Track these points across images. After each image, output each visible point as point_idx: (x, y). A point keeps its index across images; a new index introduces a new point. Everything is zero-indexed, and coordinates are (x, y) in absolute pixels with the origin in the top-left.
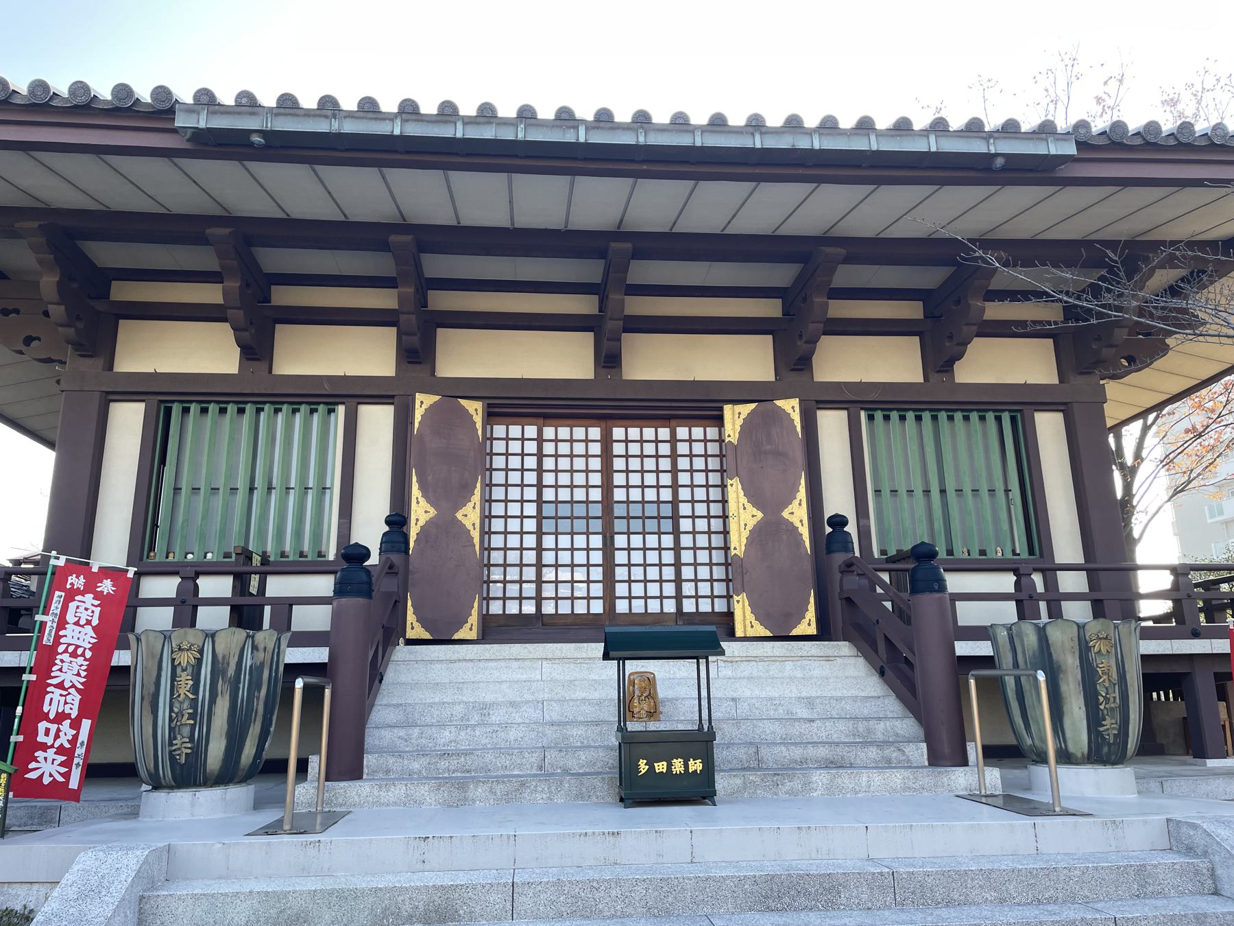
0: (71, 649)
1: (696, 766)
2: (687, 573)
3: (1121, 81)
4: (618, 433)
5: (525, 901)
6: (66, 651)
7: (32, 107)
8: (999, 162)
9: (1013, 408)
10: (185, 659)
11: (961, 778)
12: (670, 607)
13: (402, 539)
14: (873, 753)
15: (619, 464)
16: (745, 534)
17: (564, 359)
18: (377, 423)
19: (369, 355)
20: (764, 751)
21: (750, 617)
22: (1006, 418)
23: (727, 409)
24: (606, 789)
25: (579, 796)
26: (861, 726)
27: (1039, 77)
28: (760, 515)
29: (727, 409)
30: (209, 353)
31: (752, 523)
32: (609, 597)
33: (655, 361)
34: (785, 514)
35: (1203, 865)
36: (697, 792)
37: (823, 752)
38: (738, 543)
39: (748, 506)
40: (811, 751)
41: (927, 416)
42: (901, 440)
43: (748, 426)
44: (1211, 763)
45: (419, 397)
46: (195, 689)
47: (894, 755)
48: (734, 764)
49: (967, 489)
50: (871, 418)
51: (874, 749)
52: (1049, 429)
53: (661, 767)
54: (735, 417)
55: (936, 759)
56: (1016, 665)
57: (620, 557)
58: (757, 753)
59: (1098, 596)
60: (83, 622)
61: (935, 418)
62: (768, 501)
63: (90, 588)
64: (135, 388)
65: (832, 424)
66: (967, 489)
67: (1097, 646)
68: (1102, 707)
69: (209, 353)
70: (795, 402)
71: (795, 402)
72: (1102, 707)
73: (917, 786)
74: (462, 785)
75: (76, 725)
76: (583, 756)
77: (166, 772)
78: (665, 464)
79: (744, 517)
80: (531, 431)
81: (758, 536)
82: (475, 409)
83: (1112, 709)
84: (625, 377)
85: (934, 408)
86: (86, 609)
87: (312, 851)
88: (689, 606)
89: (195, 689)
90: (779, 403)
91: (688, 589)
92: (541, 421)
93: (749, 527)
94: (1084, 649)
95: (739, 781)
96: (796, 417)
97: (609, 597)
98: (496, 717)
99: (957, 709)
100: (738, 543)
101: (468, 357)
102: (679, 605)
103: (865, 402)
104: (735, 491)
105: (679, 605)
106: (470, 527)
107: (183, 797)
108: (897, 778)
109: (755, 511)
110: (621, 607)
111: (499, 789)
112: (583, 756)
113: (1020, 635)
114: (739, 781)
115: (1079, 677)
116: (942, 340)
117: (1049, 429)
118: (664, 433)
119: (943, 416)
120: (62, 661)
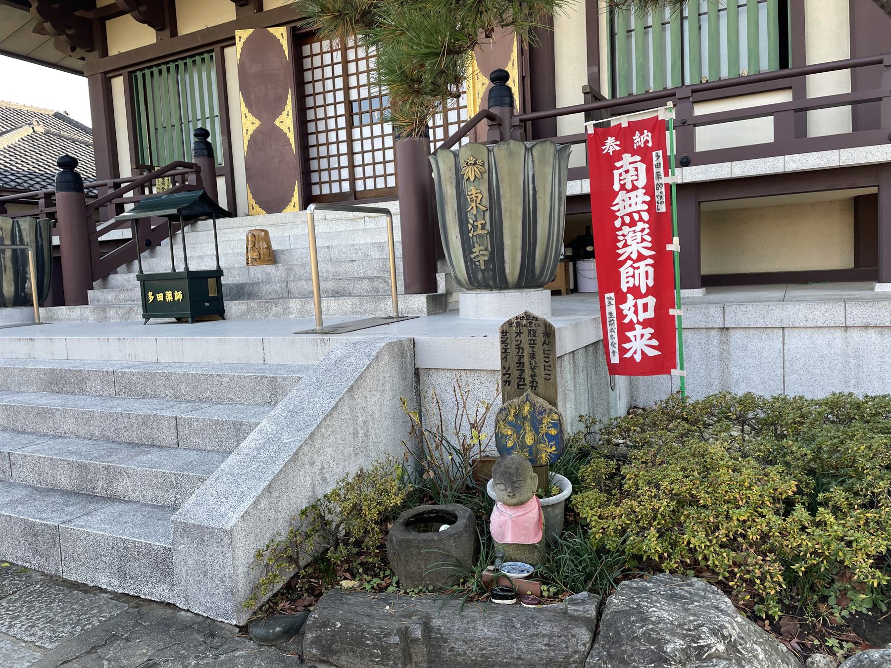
0: (627, 220)
6: (623, 223)
13: (507, 93)
16: (247, 138)
20: (292, 286)
31: (252, 129)
47: (381, 285)
48: (273, 295)
51: (366, 282)
53: (160, 297)
58: (287, 287)
60: (629, 186)
68: (471, 235)
72: (471, 235)
73: (362, 310)
83: (481, 236)
86: (627, 172)
90: (271, 30)
93: (250, 133)
95: (244, 307)
106: (286, 131)
109: (254, 119)
114: (244, 307)
115: (456, 206)
120: (624, 235)
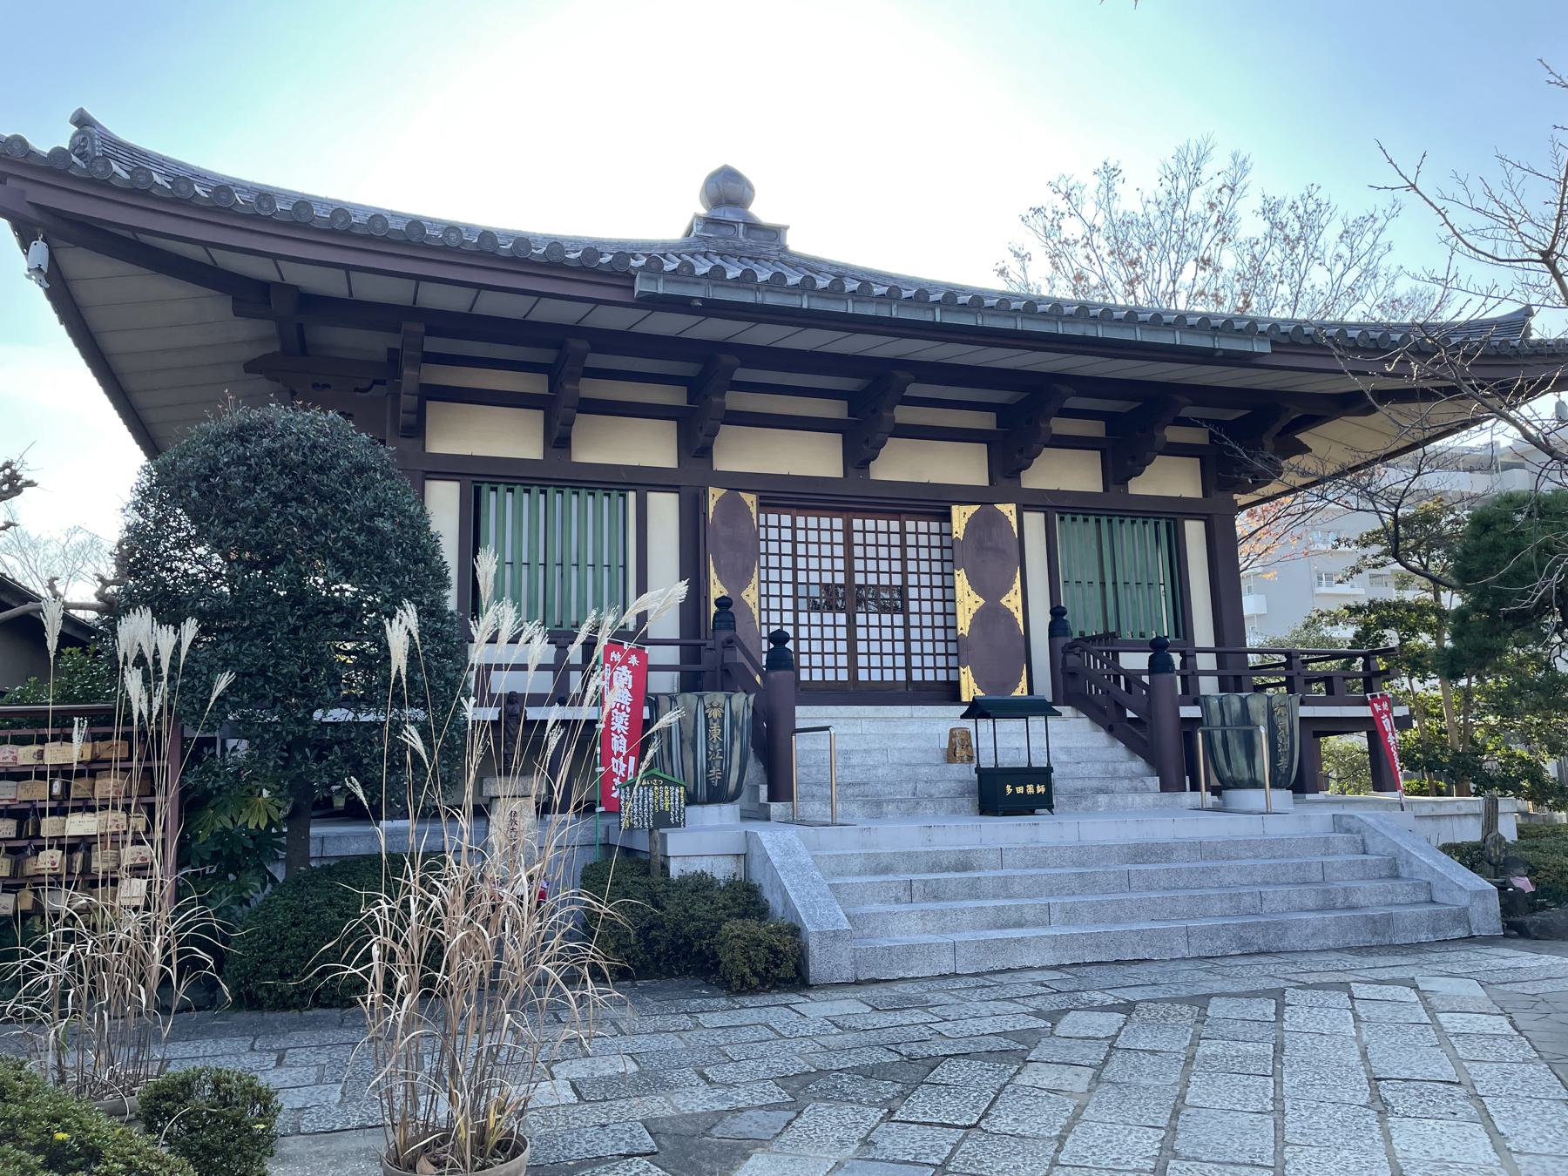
1: (1041, 789)
2: (915, 647)
3: (1232, 190)
4: (857, 524)
5: (1008, 859)
7: (513, 260)
8: (1220, 353)
9: (1169, 515)
10: (715, 713)
11: (1189, 798)
12: (901, 676)
14: (1126, 783)
15: (858, 551)
17: (818, 458)
18: (664, 509)
19: (653, 447)
21: (974, 686)
22: (1163, 524)
23: (955, 508)
24: (969, 803)
25: (954, 811)
26: (1110, 767)
27: (1164, 181)
28: (982, 601)
29: (955, 508)
30: (513, 438)
31: (975, 608)
32: (853, 667)
33: (901, 464)
34: (1003, 601)
35: (1358, 838)
36: (1045, 802)
37: (1095, 784)
38: (964, 623)
39: (973, 593)
40: (1088, 783)
41: (1104, 520)
42: (1079, 537)
43: (971, 525)
44: (1309, 797)
45: (711, 490)
46: (722, 735)
49: (1133, 583)
50: (1062, 519)
52: (1194, 532)
53: (1020, 790)
54: (961, 516)
55: (1164, 788)
56: (1223, 723)
57: (861, 633)
59: (1223, 673)
61: (1110, 521)
62: (990, 589)
63: (624, 662)
64: (448, 468)
65: (1035, 523)
66: (1133, 583)
67: (1279, 711)
69: (513, 438)
70: (1012, 507)
71: (1012, 507)
74: (879, 804)
75: (626, 761)
76: (941, 786)
77: (702, 792)
78: (896, 553)
79: (968, 603)
80: (786, 520)
81: (979, 618)
82: (750, 499)
84: (873, 477)
85: (1111, 513)
87: (866, 833)
88: (917, 676)
89: (722, 735)
90: (998, 506)
91: (916, 661)
92: (794, 511)
94: (1271, 712)
96: (1013, 520)
97: (853, 667)
98: (855, 760)
99: (1177, 755)
100: (964, 623)
101: (745, 453)
102: (909, 675)
103: (1057, 507)
104: (961, 581)
105: (909, 675)
107: (712, 809)
108: (1150, 798)
109: (978, 598)
110: (863, 676)
111: (902, 806)
112: (941, 786)
113: (1229, 704)
116: (1122, 459)
117: (1194, 532)
118: (895, 526)
119: (1116, 520)
